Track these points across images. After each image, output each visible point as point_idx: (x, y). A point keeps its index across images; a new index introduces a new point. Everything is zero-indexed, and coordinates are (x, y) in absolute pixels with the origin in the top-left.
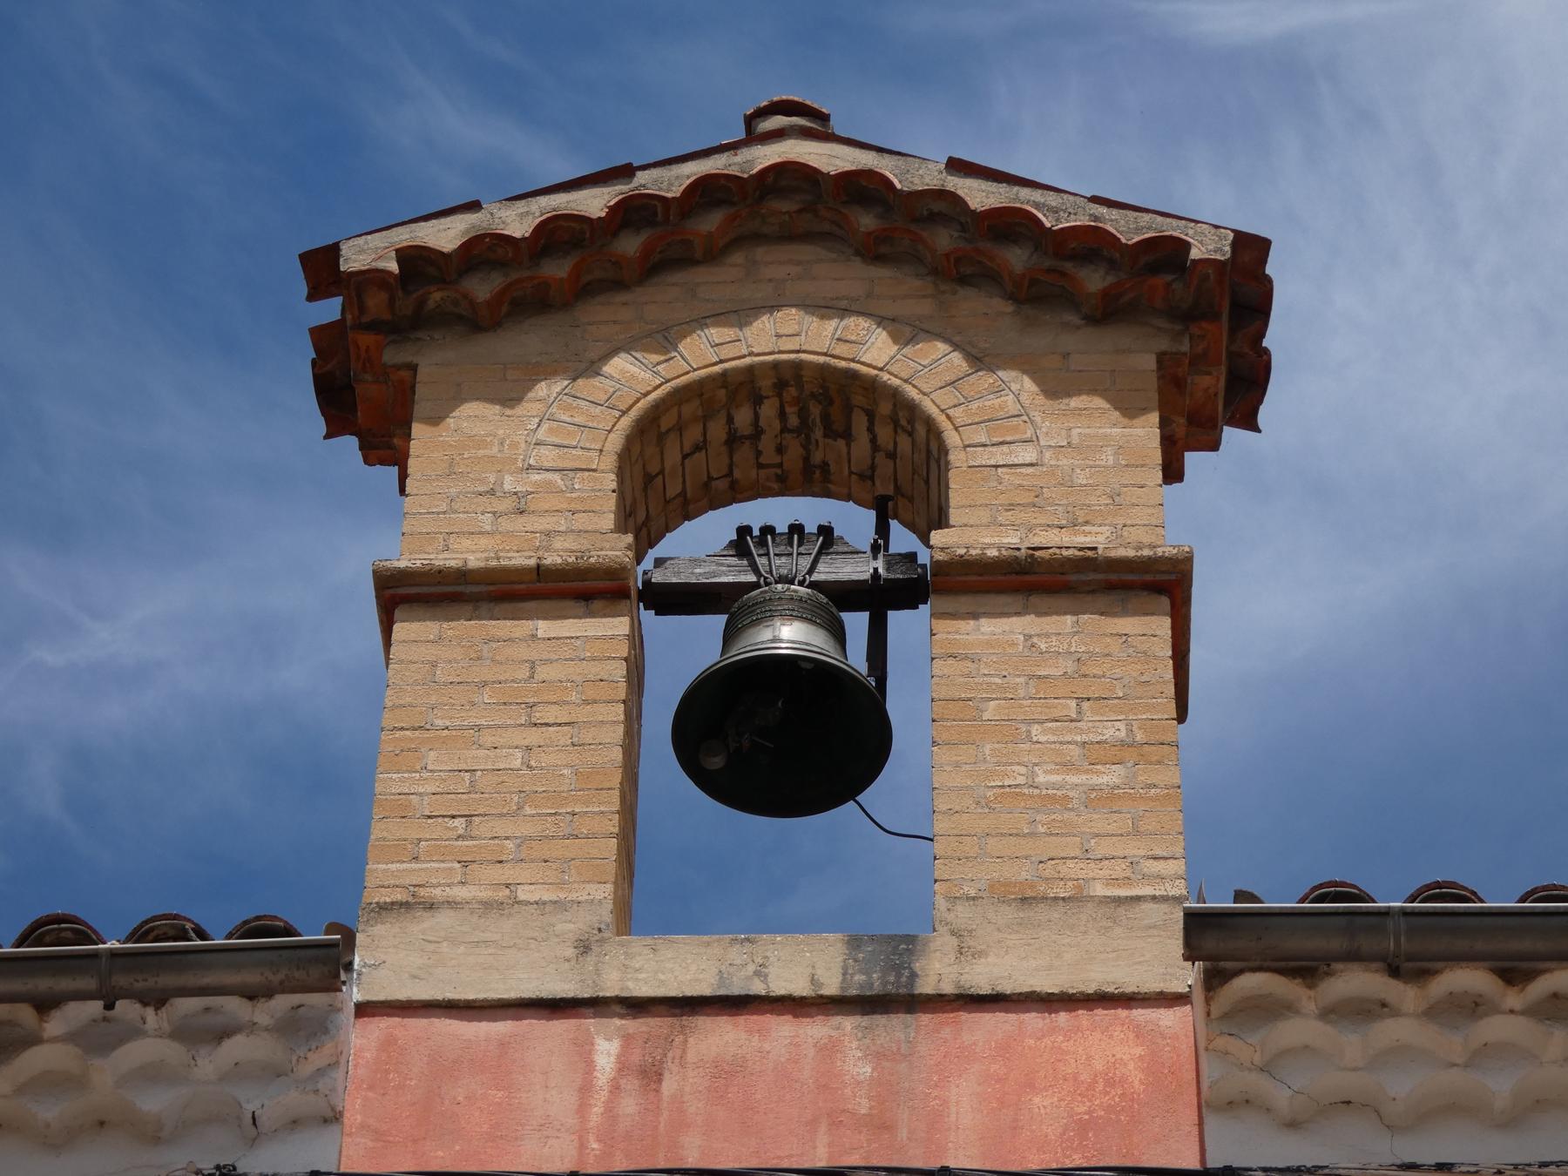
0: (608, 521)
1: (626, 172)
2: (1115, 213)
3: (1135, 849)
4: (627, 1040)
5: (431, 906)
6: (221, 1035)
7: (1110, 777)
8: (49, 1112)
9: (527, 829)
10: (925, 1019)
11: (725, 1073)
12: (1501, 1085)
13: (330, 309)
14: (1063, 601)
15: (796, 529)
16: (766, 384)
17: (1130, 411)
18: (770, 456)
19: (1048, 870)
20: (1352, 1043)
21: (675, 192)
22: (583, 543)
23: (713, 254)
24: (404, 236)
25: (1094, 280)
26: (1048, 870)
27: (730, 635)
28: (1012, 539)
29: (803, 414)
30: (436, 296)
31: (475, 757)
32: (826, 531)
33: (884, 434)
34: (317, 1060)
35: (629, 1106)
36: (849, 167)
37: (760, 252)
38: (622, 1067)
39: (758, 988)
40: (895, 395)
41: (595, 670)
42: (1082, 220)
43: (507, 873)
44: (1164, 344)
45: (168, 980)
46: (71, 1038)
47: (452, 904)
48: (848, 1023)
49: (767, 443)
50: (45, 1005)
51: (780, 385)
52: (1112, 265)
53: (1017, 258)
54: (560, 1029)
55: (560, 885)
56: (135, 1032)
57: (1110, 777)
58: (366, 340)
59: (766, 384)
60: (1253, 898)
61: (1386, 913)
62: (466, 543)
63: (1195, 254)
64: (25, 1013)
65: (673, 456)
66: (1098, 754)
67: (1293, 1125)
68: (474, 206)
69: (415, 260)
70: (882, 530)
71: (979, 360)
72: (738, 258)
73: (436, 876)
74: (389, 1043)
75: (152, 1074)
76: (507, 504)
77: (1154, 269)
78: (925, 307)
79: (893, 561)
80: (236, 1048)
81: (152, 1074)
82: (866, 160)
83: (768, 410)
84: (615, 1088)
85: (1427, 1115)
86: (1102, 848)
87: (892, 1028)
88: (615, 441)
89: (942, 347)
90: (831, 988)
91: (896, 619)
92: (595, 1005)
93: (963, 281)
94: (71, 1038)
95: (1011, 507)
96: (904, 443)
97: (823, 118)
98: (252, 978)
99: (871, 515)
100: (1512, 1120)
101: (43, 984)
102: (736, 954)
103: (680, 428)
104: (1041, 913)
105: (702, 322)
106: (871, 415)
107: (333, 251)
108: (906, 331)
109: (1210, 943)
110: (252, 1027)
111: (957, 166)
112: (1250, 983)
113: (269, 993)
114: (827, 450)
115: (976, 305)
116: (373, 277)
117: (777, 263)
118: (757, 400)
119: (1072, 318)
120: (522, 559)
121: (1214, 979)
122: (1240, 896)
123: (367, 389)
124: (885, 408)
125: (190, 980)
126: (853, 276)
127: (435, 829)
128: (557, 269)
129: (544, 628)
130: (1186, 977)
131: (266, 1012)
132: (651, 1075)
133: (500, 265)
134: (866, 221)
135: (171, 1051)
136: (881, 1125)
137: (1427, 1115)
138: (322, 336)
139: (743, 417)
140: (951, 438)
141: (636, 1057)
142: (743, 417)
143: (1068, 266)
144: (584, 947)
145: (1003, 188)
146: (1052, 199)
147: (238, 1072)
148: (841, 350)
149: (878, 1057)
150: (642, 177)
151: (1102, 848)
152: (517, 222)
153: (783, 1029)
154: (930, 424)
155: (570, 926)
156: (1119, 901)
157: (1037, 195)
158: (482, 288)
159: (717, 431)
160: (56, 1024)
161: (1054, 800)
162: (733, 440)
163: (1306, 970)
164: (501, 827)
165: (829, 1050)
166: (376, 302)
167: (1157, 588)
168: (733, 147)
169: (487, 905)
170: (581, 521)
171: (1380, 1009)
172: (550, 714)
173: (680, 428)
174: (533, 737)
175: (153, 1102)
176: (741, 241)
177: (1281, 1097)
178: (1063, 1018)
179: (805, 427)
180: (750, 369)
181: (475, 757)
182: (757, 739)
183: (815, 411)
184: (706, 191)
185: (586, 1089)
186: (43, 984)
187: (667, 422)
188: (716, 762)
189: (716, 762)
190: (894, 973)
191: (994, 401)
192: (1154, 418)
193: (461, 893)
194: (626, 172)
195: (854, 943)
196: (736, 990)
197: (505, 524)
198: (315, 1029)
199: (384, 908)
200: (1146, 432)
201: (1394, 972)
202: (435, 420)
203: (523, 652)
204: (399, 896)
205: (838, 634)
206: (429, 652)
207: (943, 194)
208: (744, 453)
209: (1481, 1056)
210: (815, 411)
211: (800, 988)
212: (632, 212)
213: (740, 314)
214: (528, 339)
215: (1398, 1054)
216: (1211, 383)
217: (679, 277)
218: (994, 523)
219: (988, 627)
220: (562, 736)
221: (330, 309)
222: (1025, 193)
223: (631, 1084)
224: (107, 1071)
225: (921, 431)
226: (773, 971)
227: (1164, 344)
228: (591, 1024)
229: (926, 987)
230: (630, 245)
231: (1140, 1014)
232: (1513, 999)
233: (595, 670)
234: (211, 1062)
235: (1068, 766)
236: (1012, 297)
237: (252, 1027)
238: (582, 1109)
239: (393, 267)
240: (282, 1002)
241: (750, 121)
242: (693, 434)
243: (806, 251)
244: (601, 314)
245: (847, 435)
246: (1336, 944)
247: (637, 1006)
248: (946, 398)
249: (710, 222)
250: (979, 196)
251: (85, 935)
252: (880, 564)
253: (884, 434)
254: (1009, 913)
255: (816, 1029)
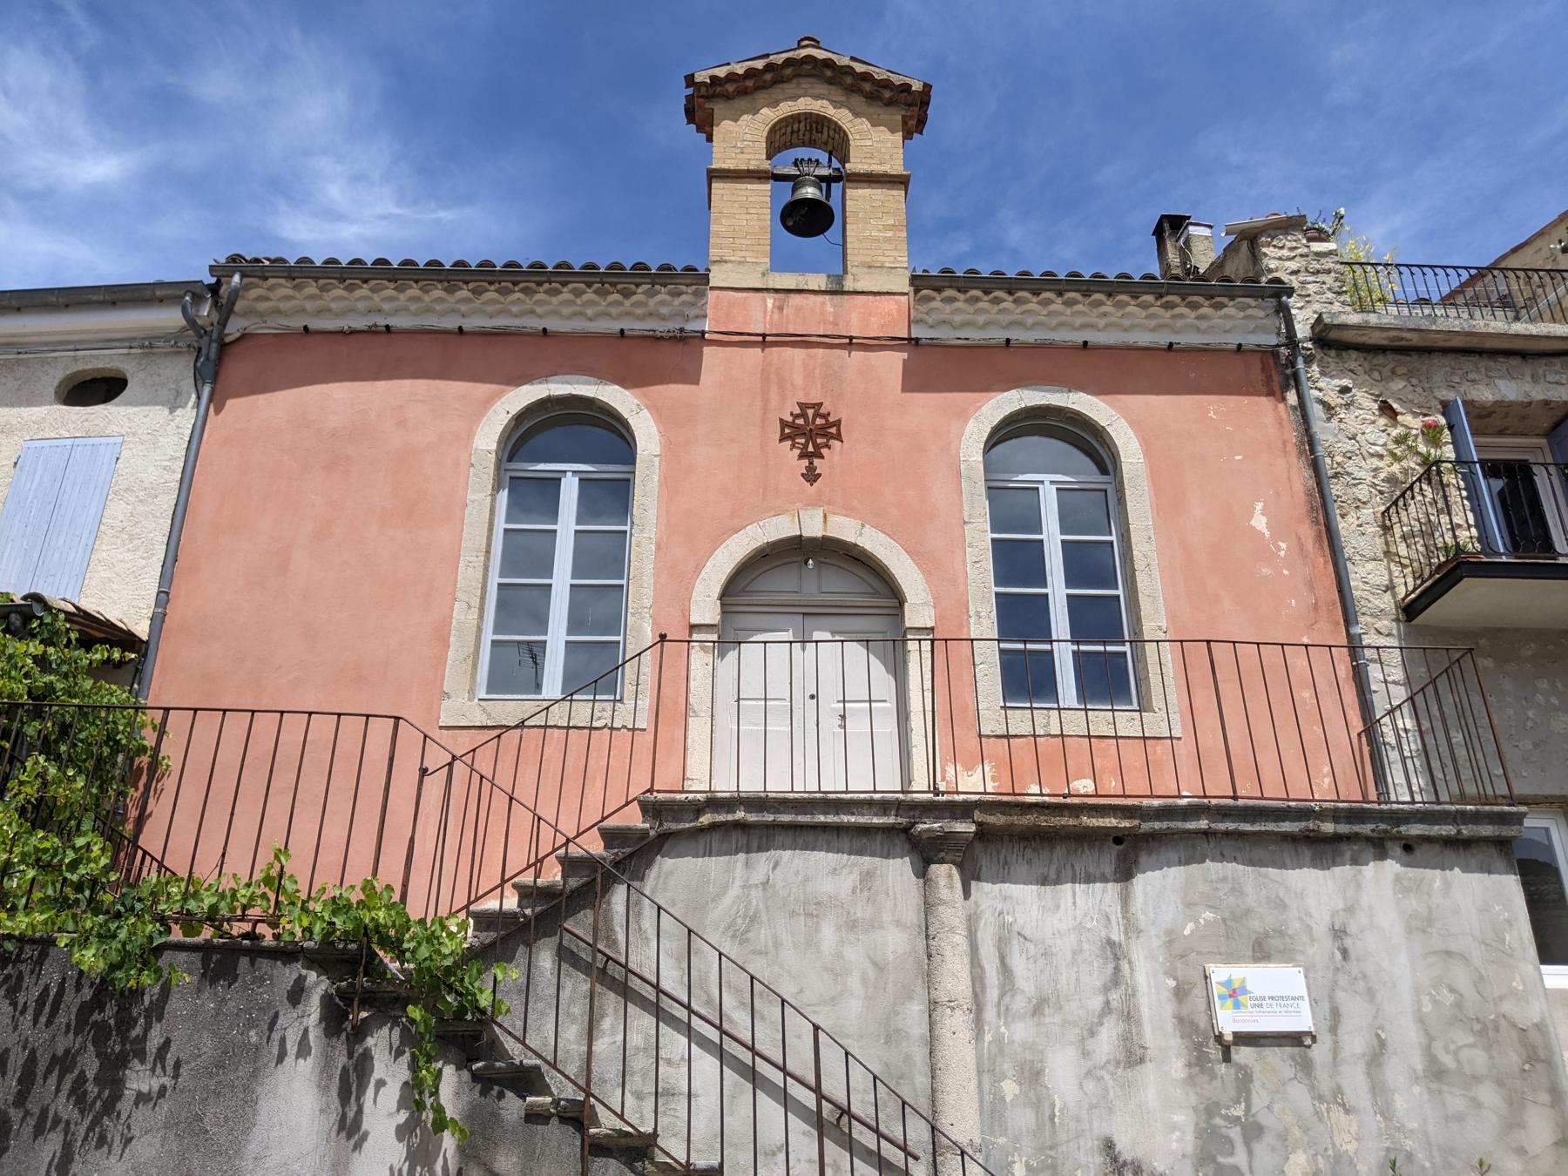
0: (764, 157)
1: (767, 56)
2: (893, 75)
3: (896, 254)
4: (775, 299)
5: (726, 262)
6: (680, 294)
7: (890, 234)
8: (639, 311)
9: (749, 242)
10: (846, 297)
11: (799, 309)
12: (981, 319)
13: (690, 91)
14: (879, 185)
15: (810, 160)
16: (802, 118)
17: (893, 131)
18: (801, 137)
19: (874, 259)
20: (948, 308)
21: (780, 63)
22: (758, 163)
23: (789, 80)
24: (711, 72)
25: (887, 94)
26: (874, 259)
27: (794, 190)
28: (866, 167)
29: (811, 126)
30: (719, 89)
31: (734, 222)
32: (817, 161)
33: (832, 133)
34: (703, 302)
35: (776, 316)
36: (824, 57)
37: (801, 80)
38: (774, 307)
39: (806, 288)
40: (836, 123)
41: (764, 199)
42: (885, 77)
43: (744, 254)
44: (903, 113)
45: (668, 281)
46: (643, 293)
47: (731, 261)
48: (827, 297)
49: (801, 133)
50: (638, 285)
51: (806, 119)
52: (892, 90)
53: (867, 86)
54: (759, 295)
55: (756, 258)
56: (659, 292)
57: (890, 234)
58: (700, 100)
59: (802, 118)
60: (928, 272)
61: (959, 277)
62: (729, 161)
63: (913, 89)
64: (633, 287)
65: (778, 137)
66: (887, 228)
67: (932, 327)
68: (728, 64)
69: (714, 78)
70: (830, 160)
71: (856, 115)
72: (795, 81)
73: (726, 254)
74: (718, 297)
75: (663, 303)
76: (739, 151)
77: (902, 92)
78: (842, 99)
79: (835, 169)
80: (683, 297)
81: (663, 303)
82: (829, 55)
83: (802, 125)
84: (772, 312)
85: (964, 325)
86: (887, 253)
87: (837, 298)
88: (765, 134)
89: (847, 111)
90: (823, 289)
91: (833, 185)
92: (767, 290)
93: (853, 91)
94: (643, 293)
95: (865, 158)
96: (837, 136)
97: (818, 42)
98: (688, 281)
99: (827, 155)
100: (983, 327)
101: (638, 280)
102: (801, 278)
103: (780, 129)
104: (873, 270)
105: (786, 99)
106: (829, 128)
107: (693, 75)
108: (837, 105)
109: (918, 282)
110: (687, 293)
111: (853, 59)
112: (924, 292)
113: (691, 285)
114: (816, 136)
115: (857, 100)
116: (703, 84)
117: (806, 83)
118: (800, 122)
119: (881, 104)
120: (743, 167)
121: (917, 291)
122: (924, 271)
123: (699, 114)
124: (833, 127)
125: (673, 281)
126: (822, 89)
127: (726, 241)
128: (749, 83)
129: (749, 186)
130: (906, 288)
131: (690, 290)
132: (781, 309)
133: (735, 81)
134: (829, 73)
135: (668, 298)
136: (835, 324)
137: (964, 325)
138: (689, 98)
139: (796, 126)
140: (850, 137)
141: (777, 304)
142: (796, 126)
143: (880, 89)
144: (764, 275)
145: (864, 66)
146: (877, 70)
147: (683, 304)
148: (822, 110)
149: (835, 306)
150: (771, 57)
151: (887, 253)
152: (740, 69)
153: (812, 297)
154: (845, 132)
155: (760, 269)
156: (892, 268)
157: (873, 69)
158: (731, 88)
159: (789, 130)
160: (639, 290)
161: (877, 240)
162: (792, 132)
163: (939, 290)
164: (742, 241)
165: (823, 304)
166: (703, 90)
167: (902, 183)
168: (794, 49)
169: (740, 262)
170: (757, 156)
171: (954, 299)
172: (753, 211)
173: (780, 129)
174: (748, 217)
175: (664, 310)
176: (795, 76)
177: (930, 321)
178: (878, 298)
179: (811, 130)
180: (799, 114)
181: (734, 222)
182: (1460, 403)
183: (814, 125)
184: (788, 62)
185: (765, 311)
186: (638, 280)
187: (777, 128)
188: (790, 224)
189: (790, 224)
190: (1506, 481)
191: (860, 127)
192: (901, 133)
193: (733, 258)
194: (767, 56)
195: (829, 276)
196: (801, 288)
197: (738, 156)
198: (702, 295)
199: (715, 262)
200: (899, 136)
201: (959, 291)
202: (717, 126)
203: (743, 193)
204: (718, 259)
205: (820, 189)
206: (722, 192)
207: (849, 67)
208: (795, 135)
209: (976, 312)
210: (814, 125)
211: (816, 288)
212: (770, 67)
213: (795, 98)
214: (742, 103)
215: (957, 310)
216: (913, 123)
217: (780, 86)
218: (861, 162)
219: (860, 191)
220: (756, 217)
221: (690, 91)
222: (870, 67)
223: (776, 311)
224: (652, 302)
225: (842, 134)
226: (809, 283)
227: (903, 113)
228: (766, 294)
229: (846, 289)
230: (768, 77)
231: (896, 297)
232: (986, 298)
233: (764, 199)
234: (677, 302)
235: (880, 231)
236: (866, 97)
237: (687, 293)
238: (765, 317)
239: (708, 81)
240: (694, 287)
241: (799, 42)
242: (783, 131)
243: (811, 80)
244: (761, 96)
245: (822, 133)
246: (947, 284)
247: (777, 291)
248: (849, 125)
249: (789, 71)
250: (859, 68)
251: (647, 268)
252: (831, 171)
253: (832, 133)
254: (866, 270)
255: (820, 298)
